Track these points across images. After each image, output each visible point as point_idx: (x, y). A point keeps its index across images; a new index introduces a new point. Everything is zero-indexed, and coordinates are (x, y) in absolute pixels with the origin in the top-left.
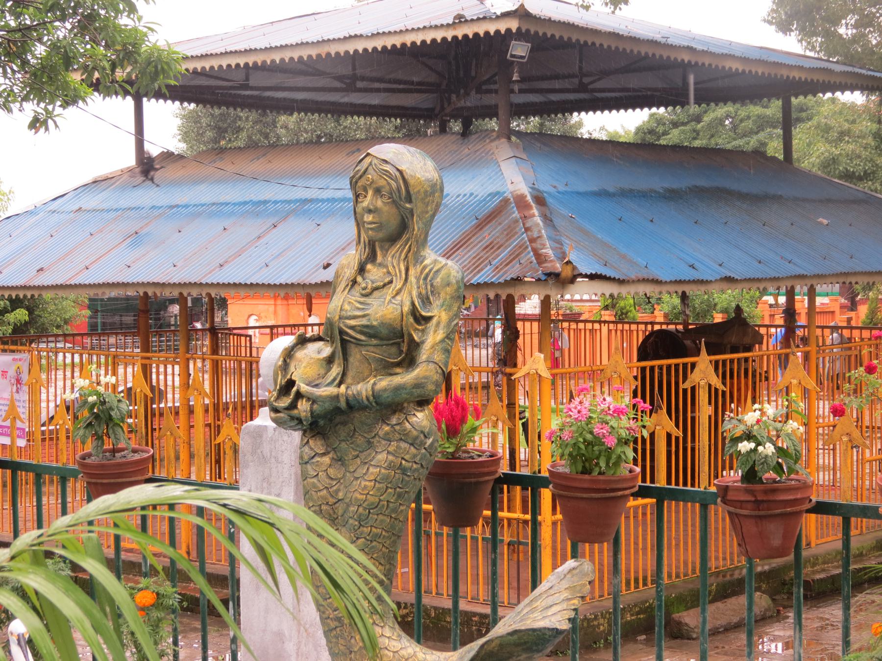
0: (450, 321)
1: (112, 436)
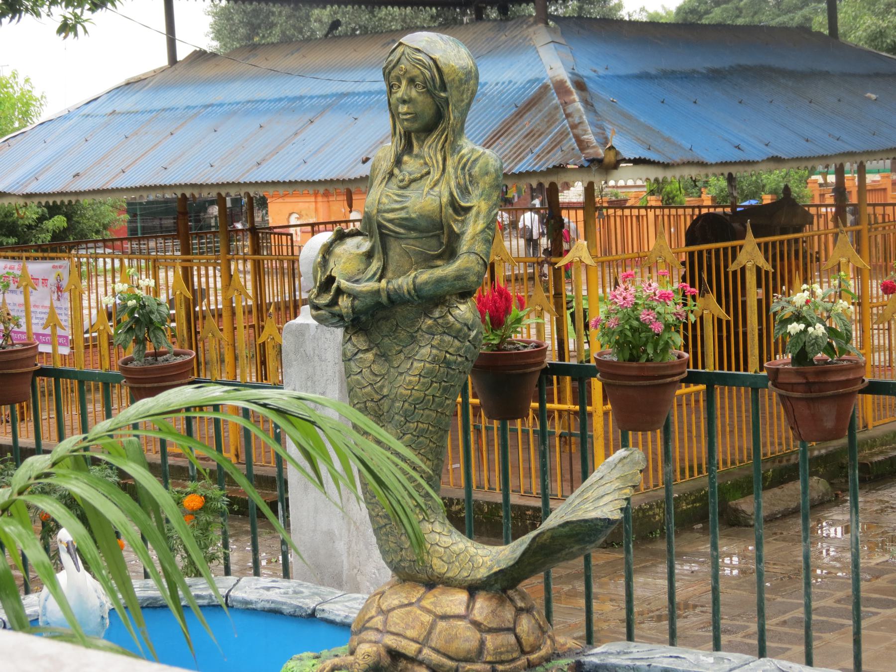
1: (154, 340)
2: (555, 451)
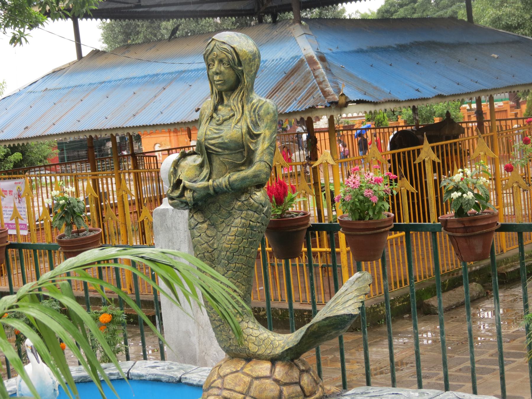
1: (76, 223)
2: (319, 276)
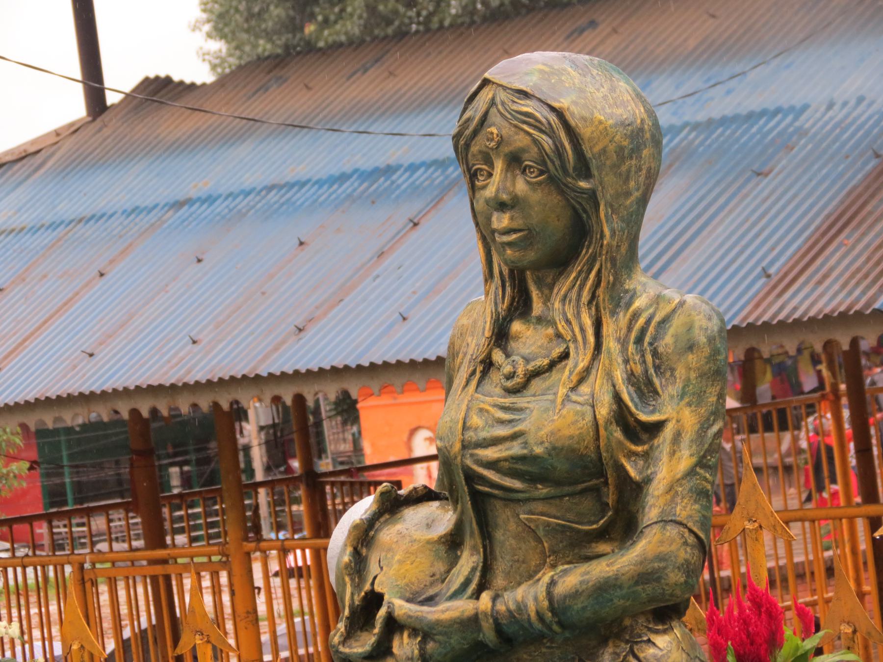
0: (704, 426)
